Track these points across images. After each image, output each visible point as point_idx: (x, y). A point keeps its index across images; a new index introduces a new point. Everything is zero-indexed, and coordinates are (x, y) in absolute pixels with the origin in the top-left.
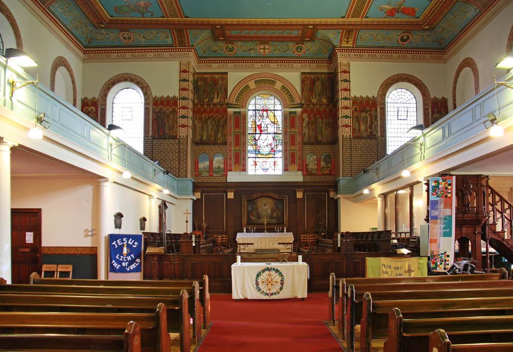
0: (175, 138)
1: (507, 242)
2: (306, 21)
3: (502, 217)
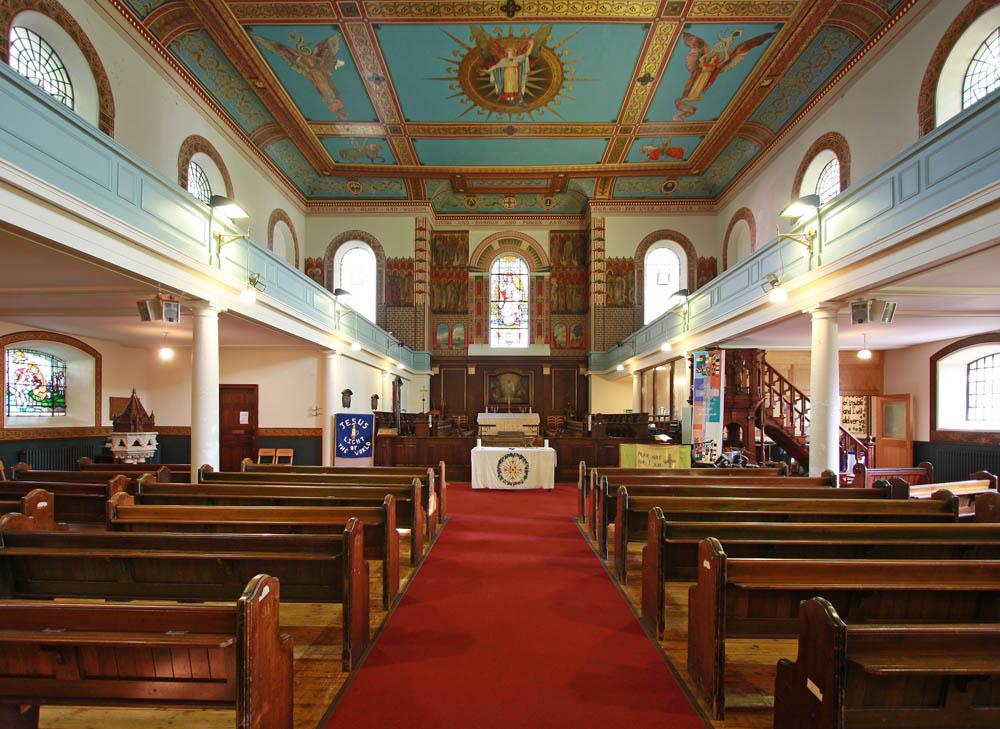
0: (411, 305)
1: (787, 431)
2: (556, 168)
3: (780, 400)
